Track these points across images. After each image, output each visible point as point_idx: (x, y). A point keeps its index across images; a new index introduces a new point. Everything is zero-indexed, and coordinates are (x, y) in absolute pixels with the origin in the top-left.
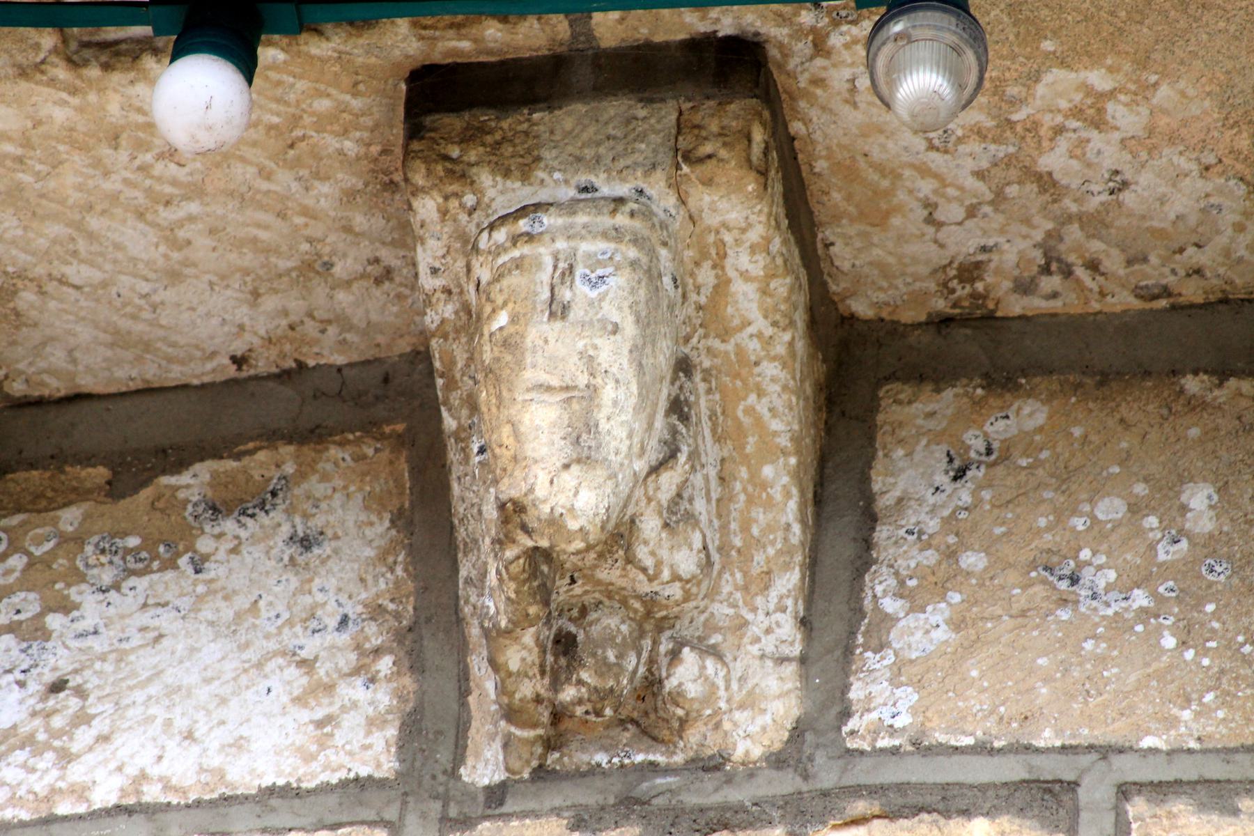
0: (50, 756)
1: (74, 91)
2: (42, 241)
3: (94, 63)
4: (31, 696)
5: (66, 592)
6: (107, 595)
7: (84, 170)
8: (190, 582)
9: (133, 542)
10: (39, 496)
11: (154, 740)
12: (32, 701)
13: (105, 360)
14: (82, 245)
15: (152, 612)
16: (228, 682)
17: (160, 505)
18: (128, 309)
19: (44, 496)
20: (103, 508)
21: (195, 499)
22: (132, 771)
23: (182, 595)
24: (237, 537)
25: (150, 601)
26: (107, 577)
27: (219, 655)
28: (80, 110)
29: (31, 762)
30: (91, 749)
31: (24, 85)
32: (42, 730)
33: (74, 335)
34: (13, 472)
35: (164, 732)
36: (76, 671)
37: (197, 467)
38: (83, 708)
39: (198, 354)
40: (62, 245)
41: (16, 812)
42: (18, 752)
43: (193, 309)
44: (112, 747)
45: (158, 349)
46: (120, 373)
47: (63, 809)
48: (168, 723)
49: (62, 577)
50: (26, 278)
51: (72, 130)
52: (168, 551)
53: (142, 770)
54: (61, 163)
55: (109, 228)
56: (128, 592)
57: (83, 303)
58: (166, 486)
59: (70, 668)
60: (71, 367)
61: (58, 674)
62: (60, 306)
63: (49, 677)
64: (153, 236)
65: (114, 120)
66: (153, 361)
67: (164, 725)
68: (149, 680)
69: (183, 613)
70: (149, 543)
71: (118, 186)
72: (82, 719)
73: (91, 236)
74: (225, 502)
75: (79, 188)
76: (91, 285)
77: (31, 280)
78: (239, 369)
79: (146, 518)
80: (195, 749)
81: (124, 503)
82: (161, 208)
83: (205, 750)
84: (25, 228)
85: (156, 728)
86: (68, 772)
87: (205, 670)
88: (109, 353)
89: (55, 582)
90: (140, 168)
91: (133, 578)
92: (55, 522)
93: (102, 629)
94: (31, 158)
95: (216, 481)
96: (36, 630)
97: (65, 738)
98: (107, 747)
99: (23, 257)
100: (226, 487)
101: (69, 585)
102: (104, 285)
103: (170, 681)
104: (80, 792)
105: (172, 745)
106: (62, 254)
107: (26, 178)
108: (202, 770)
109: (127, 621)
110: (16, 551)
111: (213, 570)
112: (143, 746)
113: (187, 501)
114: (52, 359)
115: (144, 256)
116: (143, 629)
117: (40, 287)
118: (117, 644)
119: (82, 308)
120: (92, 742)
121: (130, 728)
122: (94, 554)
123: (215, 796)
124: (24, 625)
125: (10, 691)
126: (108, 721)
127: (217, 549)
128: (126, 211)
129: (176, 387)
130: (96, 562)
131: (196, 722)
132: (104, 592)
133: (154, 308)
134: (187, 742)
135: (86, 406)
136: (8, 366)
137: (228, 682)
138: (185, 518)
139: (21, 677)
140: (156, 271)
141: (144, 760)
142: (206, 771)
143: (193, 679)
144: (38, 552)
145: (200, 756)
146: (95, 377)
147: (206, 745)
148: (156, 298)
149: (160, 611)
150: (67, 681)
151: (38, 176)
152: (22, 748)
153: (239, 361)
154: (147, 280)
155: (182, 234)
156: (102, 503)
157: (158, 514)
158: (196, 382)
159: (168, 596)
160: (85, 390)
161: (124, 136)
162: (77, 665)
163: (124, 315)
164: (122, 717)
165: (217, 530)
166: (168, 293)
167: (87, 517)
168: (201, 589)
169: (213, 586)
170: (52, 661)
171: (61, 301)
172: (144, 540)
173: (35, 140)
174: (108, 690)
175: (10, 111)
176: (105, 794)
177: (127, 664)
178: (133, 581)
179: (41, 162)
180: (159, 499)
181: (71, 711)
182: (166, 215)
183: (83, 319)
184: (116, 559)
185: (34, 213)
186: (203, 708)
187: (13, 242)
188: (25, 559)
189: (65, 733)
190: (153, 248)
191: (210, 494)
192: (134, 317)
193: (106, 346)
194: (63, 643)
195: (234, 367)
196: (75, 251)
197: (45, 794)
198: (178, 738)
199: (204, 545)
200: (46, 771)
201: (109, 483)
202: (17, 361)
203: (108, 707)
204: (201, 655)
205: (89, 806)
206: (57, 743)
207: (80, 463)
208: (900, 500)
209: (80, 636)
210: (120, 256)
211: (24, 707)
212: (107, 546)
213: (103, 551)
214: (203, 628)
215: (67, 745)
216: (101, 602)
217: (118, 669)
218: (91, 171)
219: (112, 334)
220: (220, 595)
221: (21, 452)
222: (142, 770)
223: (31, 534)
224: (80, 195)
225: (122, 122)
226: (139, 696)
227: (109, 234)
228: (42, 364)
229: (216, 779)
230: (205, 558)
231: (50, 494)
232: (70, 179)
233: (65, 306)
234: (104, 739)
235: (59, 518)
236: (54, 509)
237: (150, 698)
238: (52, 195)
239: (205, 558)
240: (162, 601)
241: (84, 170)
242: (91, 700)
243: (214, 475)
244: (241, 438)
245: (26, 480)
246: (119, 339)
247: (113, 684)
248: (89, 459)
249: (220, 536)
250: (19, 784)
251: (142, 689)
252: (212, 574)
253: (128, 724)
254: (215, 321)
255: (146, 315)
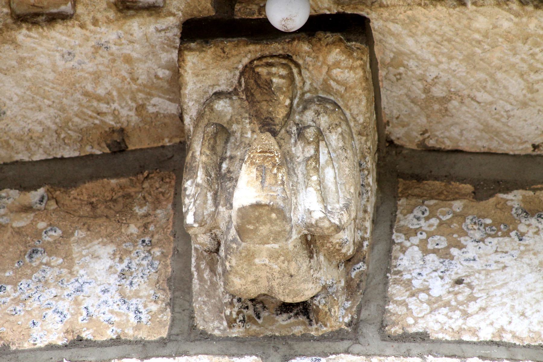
0: (458, 313)
1: (517, 15)
2: (472, 79)
3: (531, 4)
4: (447, 284)
5: (459, 239)
6: (478, 243)
7: (506, 51)
8: (517, 244)
9: (488, 221)
10: (441, 193)
11: (507, 314)
12: (447, 286)
13: (476, 137)
14: (489, 84)
15: (500, 255)
16: (539, 293)
17: (499, 206)
18: (497, 116)
19: (443, 194)
20: (472, 203)
21: (516, 206)
22: (497, 326)
23: (513, 249)
24: (537, 227)
25: (499, 250)
26: (478, 235)
27: (534, 280)
28: (517, 24)
29: (450, 314)
30: (477, 313)
31: (497, 9)
32: (453, 300)
33: (467, 124)
34: (427, 180)
35: (511, 311)
36: (467, 276)
37: (515, 192)
38: (472, 293)
39: (518, 141)
40: (480, 83)
41: (444, 335)
42: (443, 308)
43: (525, 121)
44: (488, 314)
45: (502, 136)
46: (480, 144)
47: (466, 338)
48: (513, 307)
49: (457, 232)
50: (458, 95)
51: (509, 32)
52: (505, 228)
53: (502, 327)
54: (497, 46)
55: (505, 79)
56: (488, 244)
57: (478, 110)
58: (502, 198)
59: (464, 274)
60: (459, 137)
61: (459, 276)
62: (467, 110)
63: (455, 277)
64: (523, 84)
65: (530, 31)
66: (497, 141)
67: (511, 308)
68: (502, 286)
69: (515, 258)
70: (496, 223)
71: (518, 61)
72: (472, 298)
73: (496, 81)
74: (530, 210)
75: (500, 59)
76: (485, 103)
77: (459, 96)
78: (534, 151)
79: (493, 212)
80: (527, 321)
81: (483, 203)
82: (532, 73)
83: (531, 322)
84: (468, 73)
85: (507, 308)
86: (467, 322)
87: (528, 285)
88: (479, 134)
89: (453, 234)
90: (532, 55)
91: (489, 238)
92: (451, 206)
93: (477, 259)
94: (484, 42)
95: (524, 200)
96: (447, 254)
97: (465, 306)
98: (485, 313)
99: (460, 85)
100: (530, 203)
101: (460, 236)
102: (491, 103)
103: (512, 288)
104: (474, 332)
105: (516, 317)
106: (478, 87)
107: (478, 51)
108: (530, 331)
109: (489, 257)
110: (434, 216)
111: (527, 240)
112: (502, 316)
113: (512, 207)
114: (452, 132)
115: (515, 94)
116: (496, 262)
117: (462, 100)
118: (485, 267)
119: (476, 112)
120: (477, 310)
121: (495, 306)
122: (471, 224)
123: (537, 344)
124: (440, 251)
125: (437, 280)
126: (484, 301)
127: (528, 231)
128: (516, 72)
129: (502, 154)
130: (471, 228)
131: (526, 309)
132: (477, 242)
133: (509, 117)
134: (522, 317)
135: (460, 156)
136: (431, 133)
137: (539, 293)
138: (512, 215)
139: (441, 274)
140: (517, 101)
141: (503, 322)
142: (532, 332)
143: (523, 289)
144: (444, 219)
145: (529, 325)
146: (468, 143)
147: (531, 320)
148: (511, 113)
149: (504, 255)
150: (463, 280)
151: (484, 51)
152: (445, 307)
153: (535, 147)
154: (511, 104)
155: (536, 86)
156: (472, 201)
157: (499, 211)
158: (511, 153)
159: (507, 249)
160: (460, 148)
161: (531, 39)
162: (467, 273)
163: (494, 118)
164: (491, 301)
165: (527, 223)
166: (518, 111)
167: (465, 206)
168: (522, 248)
169: (528, 248)
170: (455, 269)
171: (468, 107)
172: (494, 221)
173: (490, 34)
174: (482, 288)
175: (486, 19)
176: (486, 335)
177: (490, 277)
178: (490, 239)
179: (488, 44)
180: (499, 203)
181: (466, 294)
182: (533, 77)
183: (475, 117)
184: (482, 228)
185: (475, 67)
186: (529, 303)
187: (459, 78)
188: (438, 221)
189: (465, 304)
190: (520, 91)
191: (522, 206)
192: (498, 120)
193: (479, 130)
194: (460, 262)
195: (532, 149)
196: (485, 87)
197: (457, 329)
198: (518, 315)
199: (522, 228)
200: (457, 319)
201: (474, 193)
202: (437, 131)
203: (484, 295)
204: (524, 278)
205: (478, 339)
206: (461, 307)
207: (459, 182)
208: (42, 201)
209: (467, 260)
210: (504, 92)
211: (444, 288)
212: (477, 221)
213: (475, 223)
214: (525, 266)
215: (466, 309)
216: (476, 246)
217: (486, 279)
218: (509, 52)
219: (484, 126)
220: (532, 252)
221: (431, 172)
222: (502, 327)
223: (440, 210)
224: (499, 62)
225: (533, 32)
226: (498, 292)
227: (504, 81)
228: (447, 134)
229: (538, 336)
230: (523, 234)
231: (445, 193)
232: (497, 53)
233: (469, 110)
234: (483, 309)
235: (452, 205)
236: (449, 201)
237: (503, 294)
238: (486, 60)
239: (523, 234)
240: (504, 251)
241: (506, 51)
242: (475, 291)
243: (524, 197)
244: (535, 182)
245: (433, 185)
246: (487, 128)
247: (485, 284)
248: (463, 180)
249: (529, 225)
250: (445, 323)
251: (499, 289)
252: (527, 242)
253: (494, 304)
254: (533, 128)
255: (503, 120)
